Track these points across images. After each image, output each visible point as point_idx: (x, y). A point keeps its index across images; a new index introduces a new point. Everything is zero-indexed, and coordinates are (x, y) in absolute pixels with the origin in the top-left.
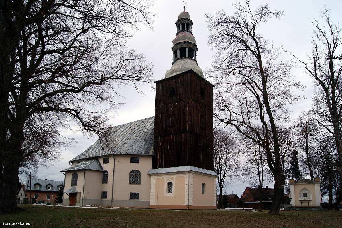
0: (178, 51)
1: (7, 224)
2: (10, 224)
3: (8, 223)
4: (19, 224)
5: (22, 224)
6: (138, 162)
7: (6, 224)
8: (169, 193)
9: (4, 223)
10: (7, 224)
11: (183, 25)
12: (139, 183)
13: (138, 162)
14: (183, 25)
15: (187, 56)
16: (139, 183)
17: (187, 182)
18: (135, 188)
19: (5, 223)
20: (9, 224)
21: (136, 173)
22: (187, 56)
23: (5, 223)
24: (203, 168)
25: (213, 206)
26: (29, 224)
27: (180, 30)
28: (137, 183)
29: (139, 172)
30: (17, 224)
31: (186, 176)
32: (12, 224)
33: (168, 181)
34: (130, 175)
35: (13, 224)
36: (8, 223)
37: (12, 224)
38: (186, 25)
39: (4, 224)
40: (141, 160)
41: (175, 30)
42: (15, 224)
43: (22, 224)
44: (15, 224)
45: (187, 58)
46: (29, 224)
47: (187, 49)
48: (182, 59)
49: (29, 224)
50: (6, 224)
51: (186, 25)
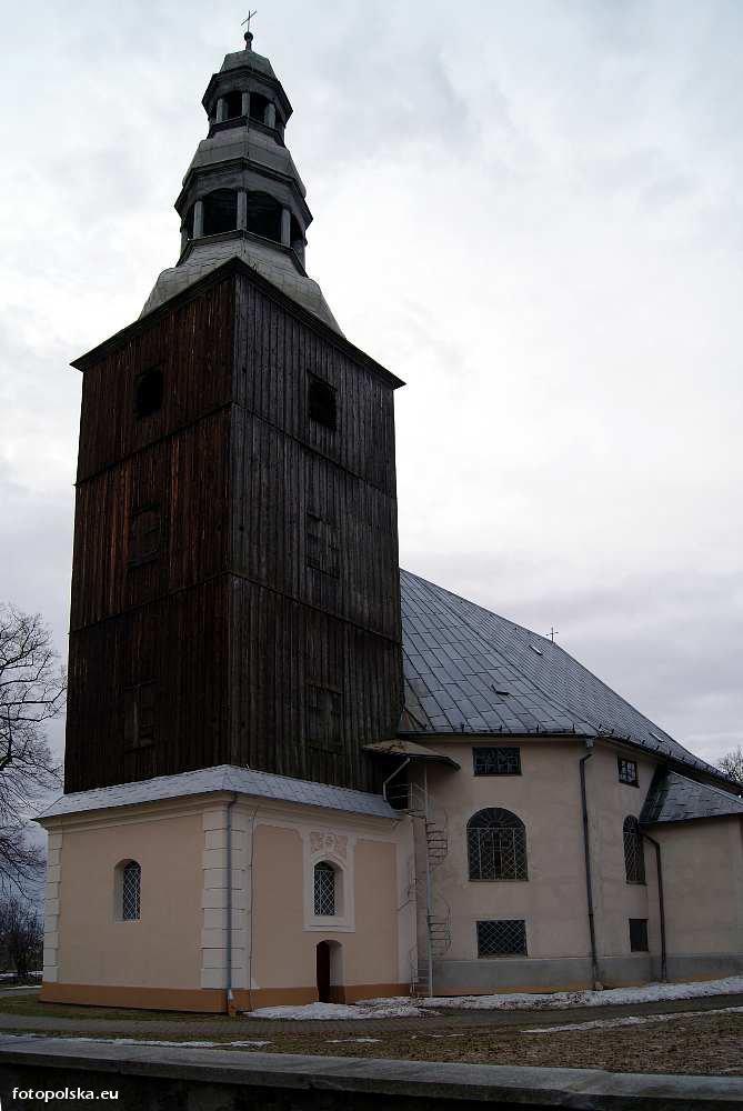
0: (198, 210)
1: (29, 1094)
2: (40, 1095)
3: (31, 1091)
4: (76, 1094)
5: (84, 1095)
6: (517, 771)
7: (23, 1095)
8: (125, 919)
9: (15, 1092)
10: (29, 1094)
11: (233, 100)
12: (522, 876)
13: (517, 771)
14: (233, 100)
15: (241, 223)
16: (522, 876)
17: (213, 860)
18: (498, 900)
19: (19, 1091)
20: (33, 1095)
21: (498, 825)
22: (241, 223)
23: (19, 1091)
24: (142, 774)
25: (199, 988)
26: (114, 1095)
27: (219, 119)
28: (509, 877)
29: (515, 817)
30: (65, 1095)
31: (214, 819)
32: (45, 1096)
33: (320, 857)
34: (470, 835)
35: (50, 1095)
36: (31, 1091)
37: (45, 1096)
38: (245, 99)
39: (17, 1094)
40: (528, 761)
41: (200, 126)
42: (60, 1095)
43: (84, 1095)
44: (60, 1095)
45: (240, 235)
46: (114, 1095)
47: (242, 199)
48: (255, 240)
49: (112, 1097)
50: (23, 1095)
51: (245, 99)
